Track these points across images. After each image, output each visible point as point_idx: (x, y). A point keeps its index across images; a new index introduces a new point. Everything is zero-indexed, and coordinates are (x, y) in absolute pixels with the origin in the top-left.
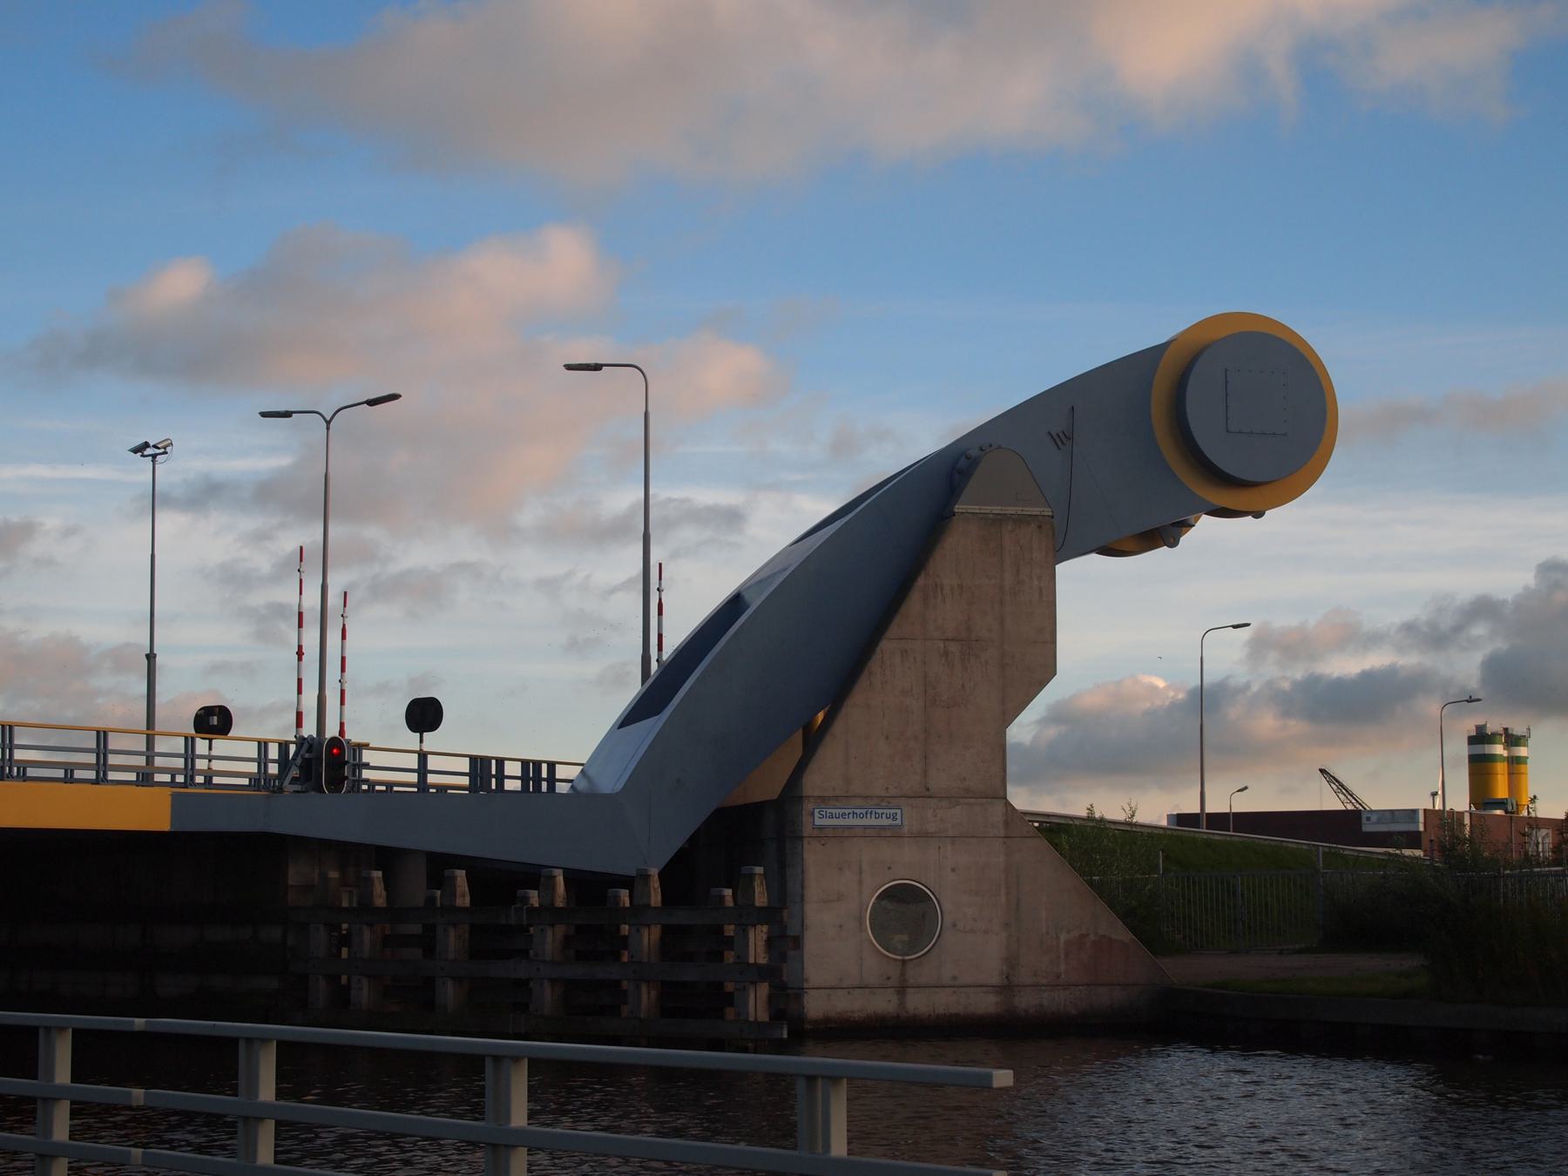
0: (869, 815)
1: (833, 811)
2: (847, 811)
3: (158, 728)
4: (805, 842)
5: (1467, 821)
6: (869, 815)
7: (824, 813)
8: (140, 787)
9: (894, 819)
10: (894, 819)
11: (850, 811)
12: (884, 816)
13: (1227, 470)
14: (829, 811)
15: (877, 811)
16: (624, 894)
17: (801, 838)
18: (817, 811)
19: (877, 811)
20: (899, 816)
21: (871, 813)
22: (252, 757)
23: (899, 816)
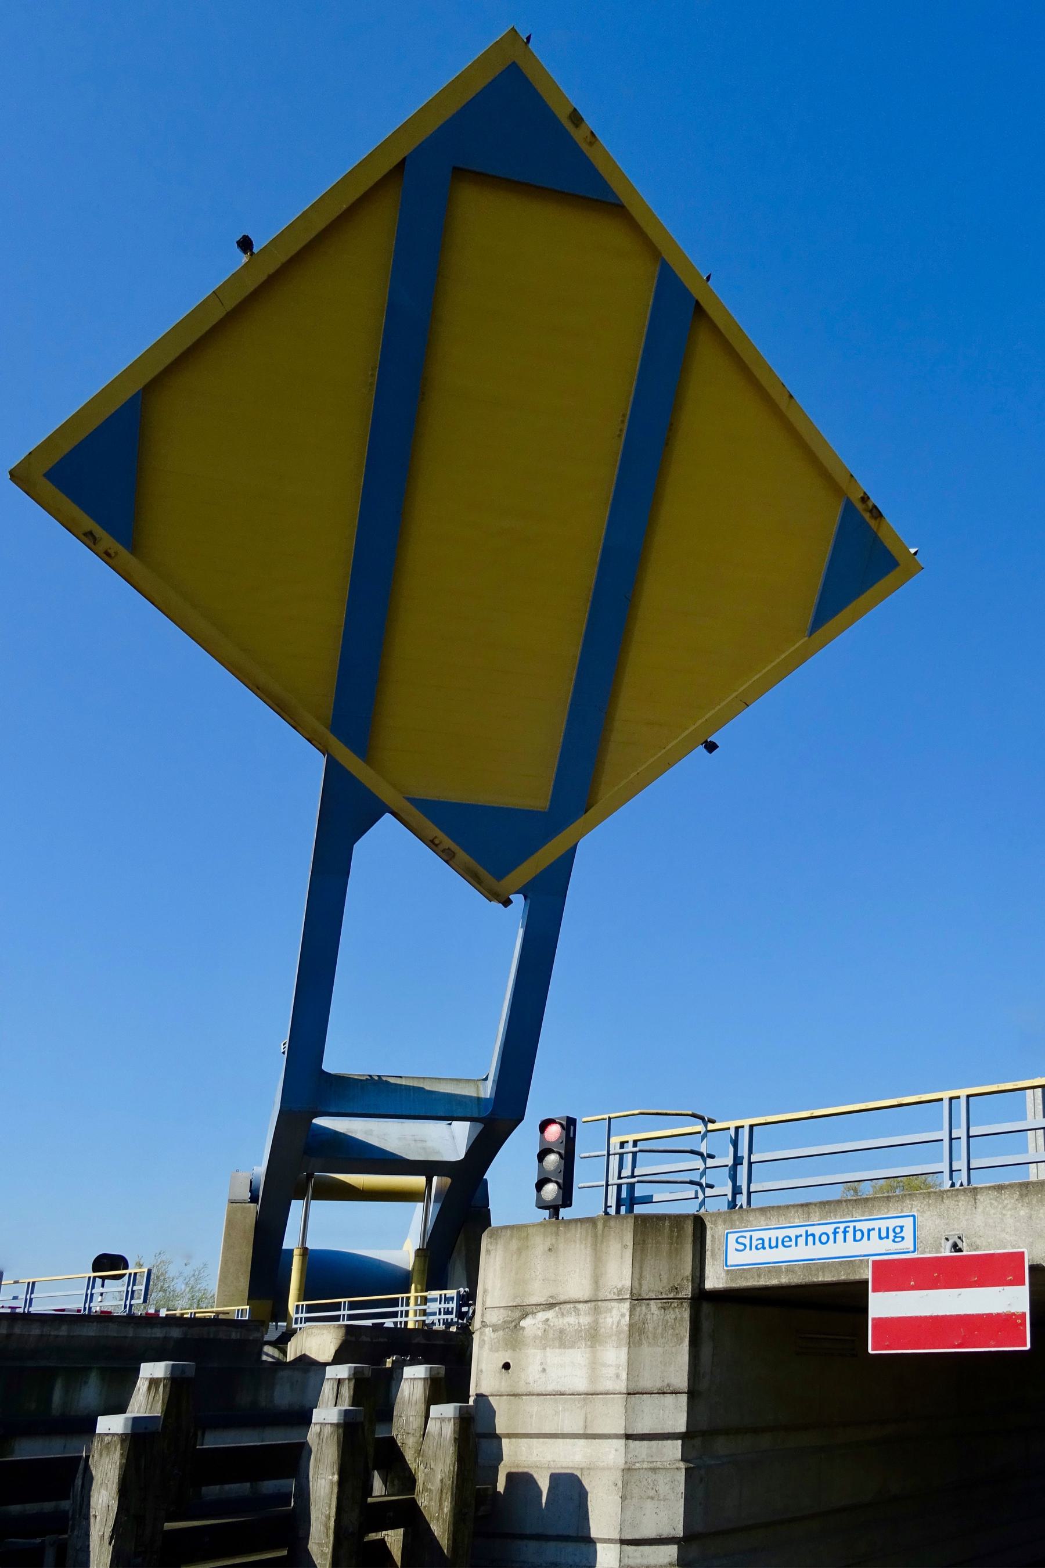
0: (840, 1236)
1: (765, 1235)
2: (792, 1233)
3: (1038, 1164)
4: (686, 1390)
5: (384, 1367)
6: (840, 1236)
7: (747, 1242)
8: (776, 1205)
9: (898, 1237)
10: (898, 1236)
11: (802, 1231)
12: (874, 1234)
13: (601, 172)
14: (756, 1235)
15: (859, 1226)
16: (1014, 1317)
17: (498, 1438)
18: (732, 1238)
19: (859, 1226)
20: (908, 1233)
21: (845, 1232)
22: (953, 1167)
23: (908, 1233)
